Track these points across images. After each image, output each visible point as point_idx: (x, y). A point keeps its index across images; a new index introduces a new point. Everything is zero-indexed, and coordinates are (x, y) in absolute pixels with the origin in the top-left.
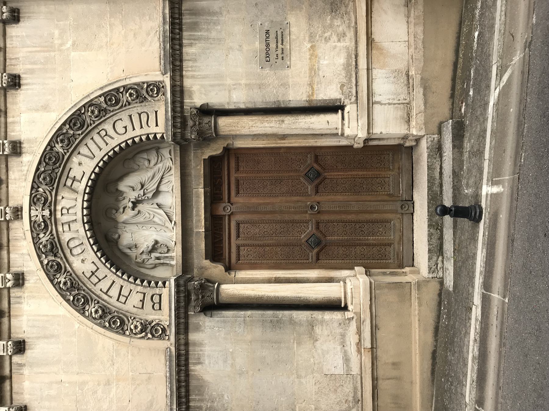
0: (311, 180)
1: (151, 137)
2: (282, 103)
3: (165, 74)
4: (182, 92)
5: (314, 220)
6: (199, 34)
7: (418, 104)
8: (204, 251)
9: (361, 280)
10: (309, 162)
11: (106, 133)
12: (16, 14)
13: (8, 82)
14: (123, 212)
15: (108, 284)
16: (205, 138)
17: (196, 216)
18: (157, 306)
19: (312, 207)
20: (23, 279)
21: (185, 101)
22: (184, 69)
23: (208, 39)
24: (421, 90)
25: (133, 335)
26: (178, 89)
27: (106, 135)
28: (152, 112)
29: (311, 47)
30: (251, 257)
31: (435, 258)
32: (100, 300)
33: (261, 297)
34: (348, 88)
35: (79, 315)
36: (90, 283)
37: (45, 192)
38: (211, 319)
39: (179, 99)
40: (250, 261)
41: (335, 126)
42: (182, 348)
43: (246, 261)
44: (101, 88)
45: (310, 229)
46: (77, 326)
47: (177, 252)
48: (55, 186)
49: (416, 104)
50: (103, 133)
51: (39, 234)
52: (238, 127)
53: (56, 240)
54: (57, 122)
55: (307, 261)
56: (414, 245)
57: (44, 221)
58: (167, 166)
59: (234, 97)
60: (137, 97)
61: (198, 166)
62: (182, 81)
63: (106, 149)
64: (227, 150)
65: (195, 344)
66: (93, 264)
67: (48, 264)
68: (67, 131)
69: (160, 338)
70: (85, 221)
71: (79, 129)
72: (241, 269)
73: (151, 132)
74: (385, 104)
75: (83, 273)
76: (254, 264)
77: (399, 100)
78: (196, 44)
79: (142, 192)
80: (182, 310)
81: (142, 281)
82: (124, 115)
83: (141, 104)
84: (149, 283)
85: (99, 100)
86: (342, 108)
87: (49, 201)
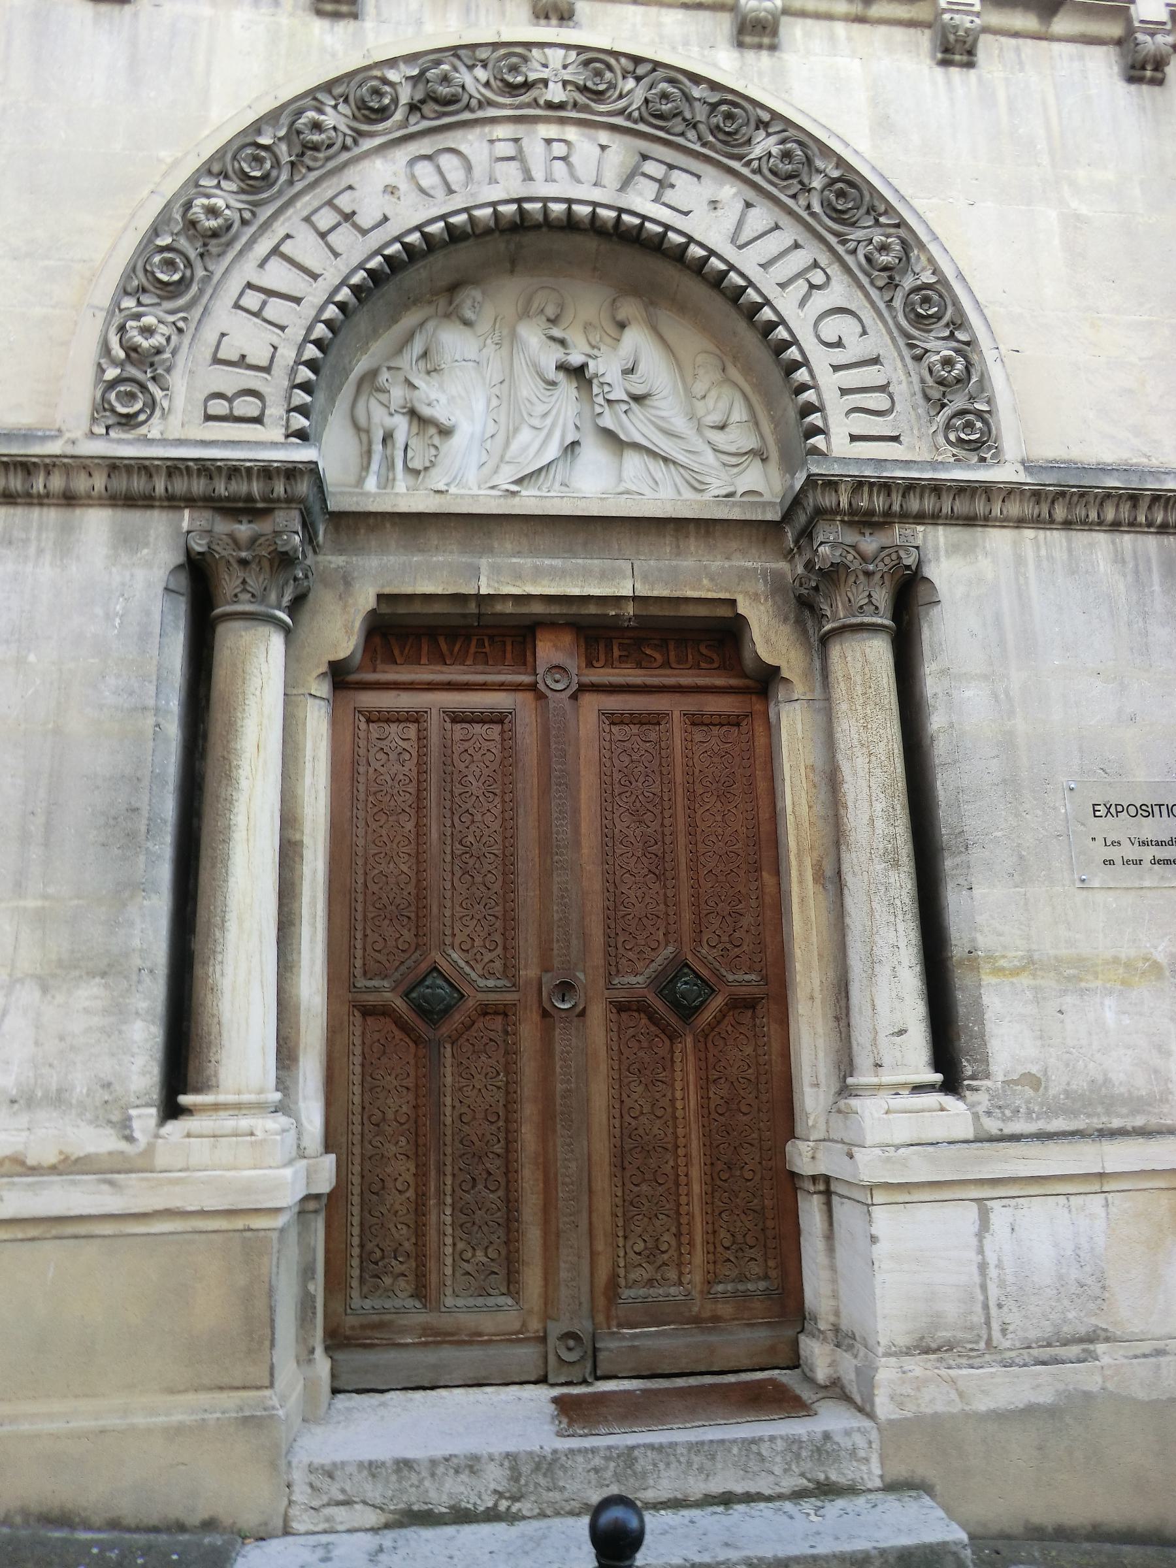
0: (665, 984)
1: (815, 419)
2: (958, 860)
3: (1026, 469)
4: (970, 521)
5: (515, 996)
6: (1157, 588)
7: (1001, 1388)
8: (408, 590)
9: (288, 1172)
10: (731, 978)
11: (818, 287)
12: (1148, 73)
13: (956, 27)
14: (553, 339)
15: (307, 259)
16: (806, 606)
17: (536, 567)
18: (219, 407)
19: (566, 988)
20: (336, 16)
21: (941, 530)
22: (1041, 532)
23: (1145, 615)
24: (1045, 1397)
25: (118, 320)
26: (980, 507)
27: (812, 286)
28: (895, 427)
29: (1156, 967)
30: (376, 765)
31: (374, 1492)
32: (250, 231)
33: (229, 777)
34: (1028, 1102)
35: (206, 155)
36: (316, 204)
37: (621, 97)
38: (160, 590)
39: (946, 509)
40: (363, 761)
41: (886, 1061)
42: (57, 482)
43: (362, 743)
44: (960, 276)
45: (482, 983)
46: (167, 155)
47: (407, 497)
48: (642, 127)
49: (992, 1376)
50: (817, 277)
51: (485, 66)
52: (865, 704)
53: (467, 116)
54: (847, 145)
55: (358, 972)
56: (419, 1395)
57: (527, 85)
58: (708, 480)
59: (968, 694)
60: (941, 382)
61: (712, 579)
62: (1004, 522)
63: (767, 282)
64: (766, 681)
65: (67, 529)
66: (379, 217)
67: (385, 81)
68: (819, 171)
69: (102, 407)
70: (527, 206)
71: (826, 204)
72: (335, 722)
73: (831, 421)
74: (981, 1251)
75: (350, 187)
76: (355, 772)
77: (1000, 1306)
78: (1125, 575)
79: (618, 394)
80: (199, 486)
81: (312, 365)
82: (879, 341)
83: (919, 396)
84: (306, 387)
85: (924, 269)
86: (951, 1084)
87: (593, 104)
